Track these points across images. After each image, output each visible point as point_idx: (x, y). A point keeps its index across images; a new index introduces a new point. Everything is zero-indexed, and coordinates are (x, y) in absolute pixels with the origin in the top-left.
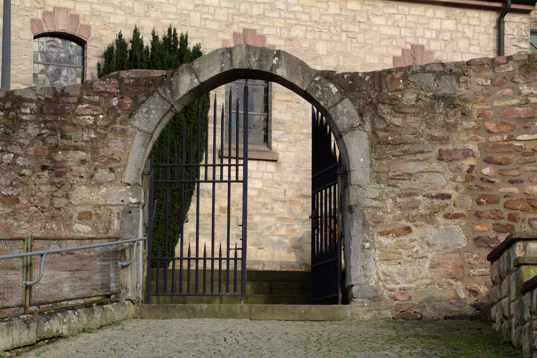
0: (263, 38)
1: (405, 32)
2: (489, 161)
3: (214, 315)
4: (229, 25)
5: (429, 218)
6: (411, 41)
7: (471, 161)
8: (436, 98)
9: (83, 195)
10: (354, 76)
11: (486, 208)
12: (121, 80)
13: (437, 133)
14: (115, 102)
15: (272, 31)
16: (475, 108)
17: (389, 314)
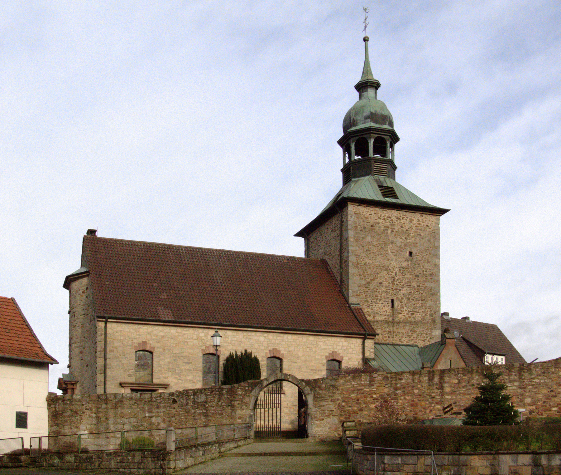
0: (279, 351)
1: (330, 347)
2: (344, 401)
3: (273, 441)
4: (268, 347)
5: (328, 416)
6: (332, 350)
7: (339, 402)
8: (331, 386)
9: (239, 412)
10: (309, 380)
11: (343, 413)
12: (248, 383)
13: (331, 395)
14: (247, 388)
15: (283, 349)
16: (340, 388)
17: (318, 440)
